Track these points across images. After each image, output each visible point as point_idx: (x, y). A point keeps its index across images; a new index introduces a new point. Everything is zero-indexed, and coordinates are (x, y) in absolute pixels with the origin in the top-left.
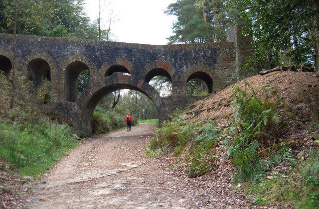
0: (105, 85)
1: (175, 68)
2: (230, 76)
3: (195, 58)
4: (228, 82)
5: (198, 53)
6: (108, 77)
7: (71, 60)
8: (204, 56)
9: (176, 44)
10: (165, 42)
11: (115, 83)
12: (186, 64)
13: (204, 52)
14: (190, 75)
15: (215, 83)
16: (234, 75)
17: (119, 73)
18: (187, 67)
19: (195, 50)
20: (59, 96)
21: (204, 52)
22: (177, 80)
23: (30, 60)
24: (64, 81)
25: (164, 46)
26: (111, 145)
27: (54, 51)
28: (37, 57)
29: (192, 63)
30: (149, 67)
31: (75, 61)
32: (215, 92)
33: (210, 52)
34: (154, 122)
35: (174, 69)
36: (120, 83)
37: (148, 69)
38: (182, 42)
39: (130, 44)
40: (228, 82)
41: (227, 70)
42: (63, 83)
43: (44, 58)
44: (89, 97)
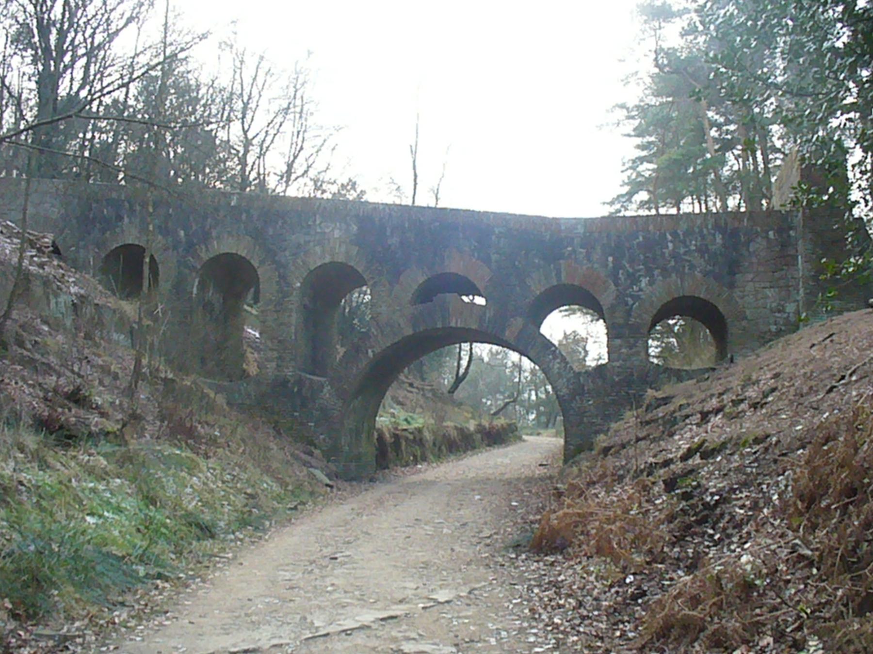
0: (409, 332)
1: (617, 285)
2: (779, 312)
3: (675, 255)
4: (773, 328)
5: (684, 242)
6: (420, 307)
7: (318, 258)
8: (702, 250)
9: (628, 214)
10: (605, 211)
11: (439, 326)
12: (649, 272)
13: (703, 237)
14: (659, 305)
15: (734, 329)
16: (790, 308)
17: (450, 297)
18: (651, 283)
19: (675, 234)
20: (280, 358)
21: (703, 237)
22: (621, 321)
23: (205, 256)
24: (294, 315)
25: (589, 223)
26: (416, 506)
27: (271, 233)
28: (224, 250)
29: (665, 272)
30: (540, 282)
31: (327, 260)
32: (732, 361)
33: (719, 238)
34: (705, 409)
35: (613, 287)
36: (453, 324)
37: (537, 286)
38: (649, 209)
39: (486, 213)
40: (773, 328)
41: (769, 292)
42: (294, 322)
43: (243, 253)
44: (363, 364)
